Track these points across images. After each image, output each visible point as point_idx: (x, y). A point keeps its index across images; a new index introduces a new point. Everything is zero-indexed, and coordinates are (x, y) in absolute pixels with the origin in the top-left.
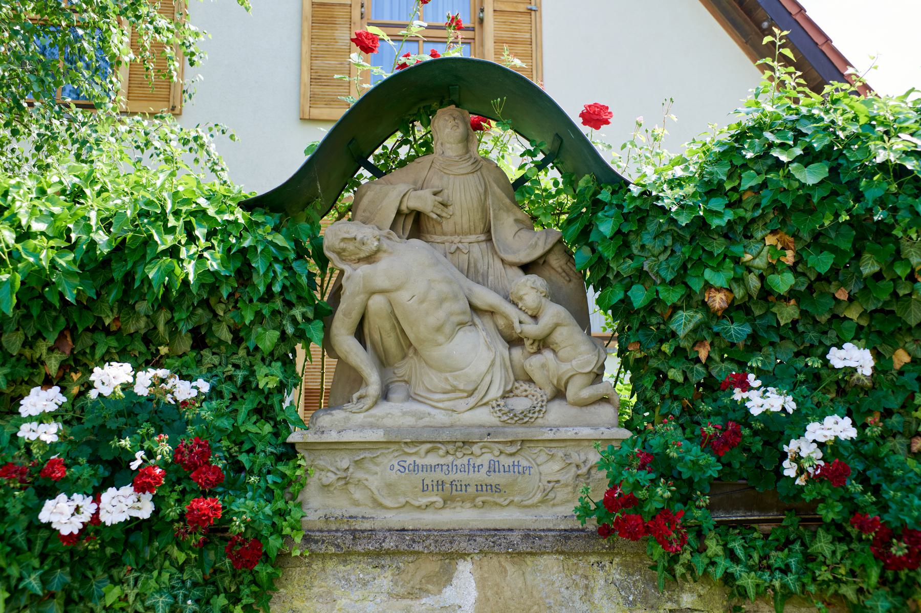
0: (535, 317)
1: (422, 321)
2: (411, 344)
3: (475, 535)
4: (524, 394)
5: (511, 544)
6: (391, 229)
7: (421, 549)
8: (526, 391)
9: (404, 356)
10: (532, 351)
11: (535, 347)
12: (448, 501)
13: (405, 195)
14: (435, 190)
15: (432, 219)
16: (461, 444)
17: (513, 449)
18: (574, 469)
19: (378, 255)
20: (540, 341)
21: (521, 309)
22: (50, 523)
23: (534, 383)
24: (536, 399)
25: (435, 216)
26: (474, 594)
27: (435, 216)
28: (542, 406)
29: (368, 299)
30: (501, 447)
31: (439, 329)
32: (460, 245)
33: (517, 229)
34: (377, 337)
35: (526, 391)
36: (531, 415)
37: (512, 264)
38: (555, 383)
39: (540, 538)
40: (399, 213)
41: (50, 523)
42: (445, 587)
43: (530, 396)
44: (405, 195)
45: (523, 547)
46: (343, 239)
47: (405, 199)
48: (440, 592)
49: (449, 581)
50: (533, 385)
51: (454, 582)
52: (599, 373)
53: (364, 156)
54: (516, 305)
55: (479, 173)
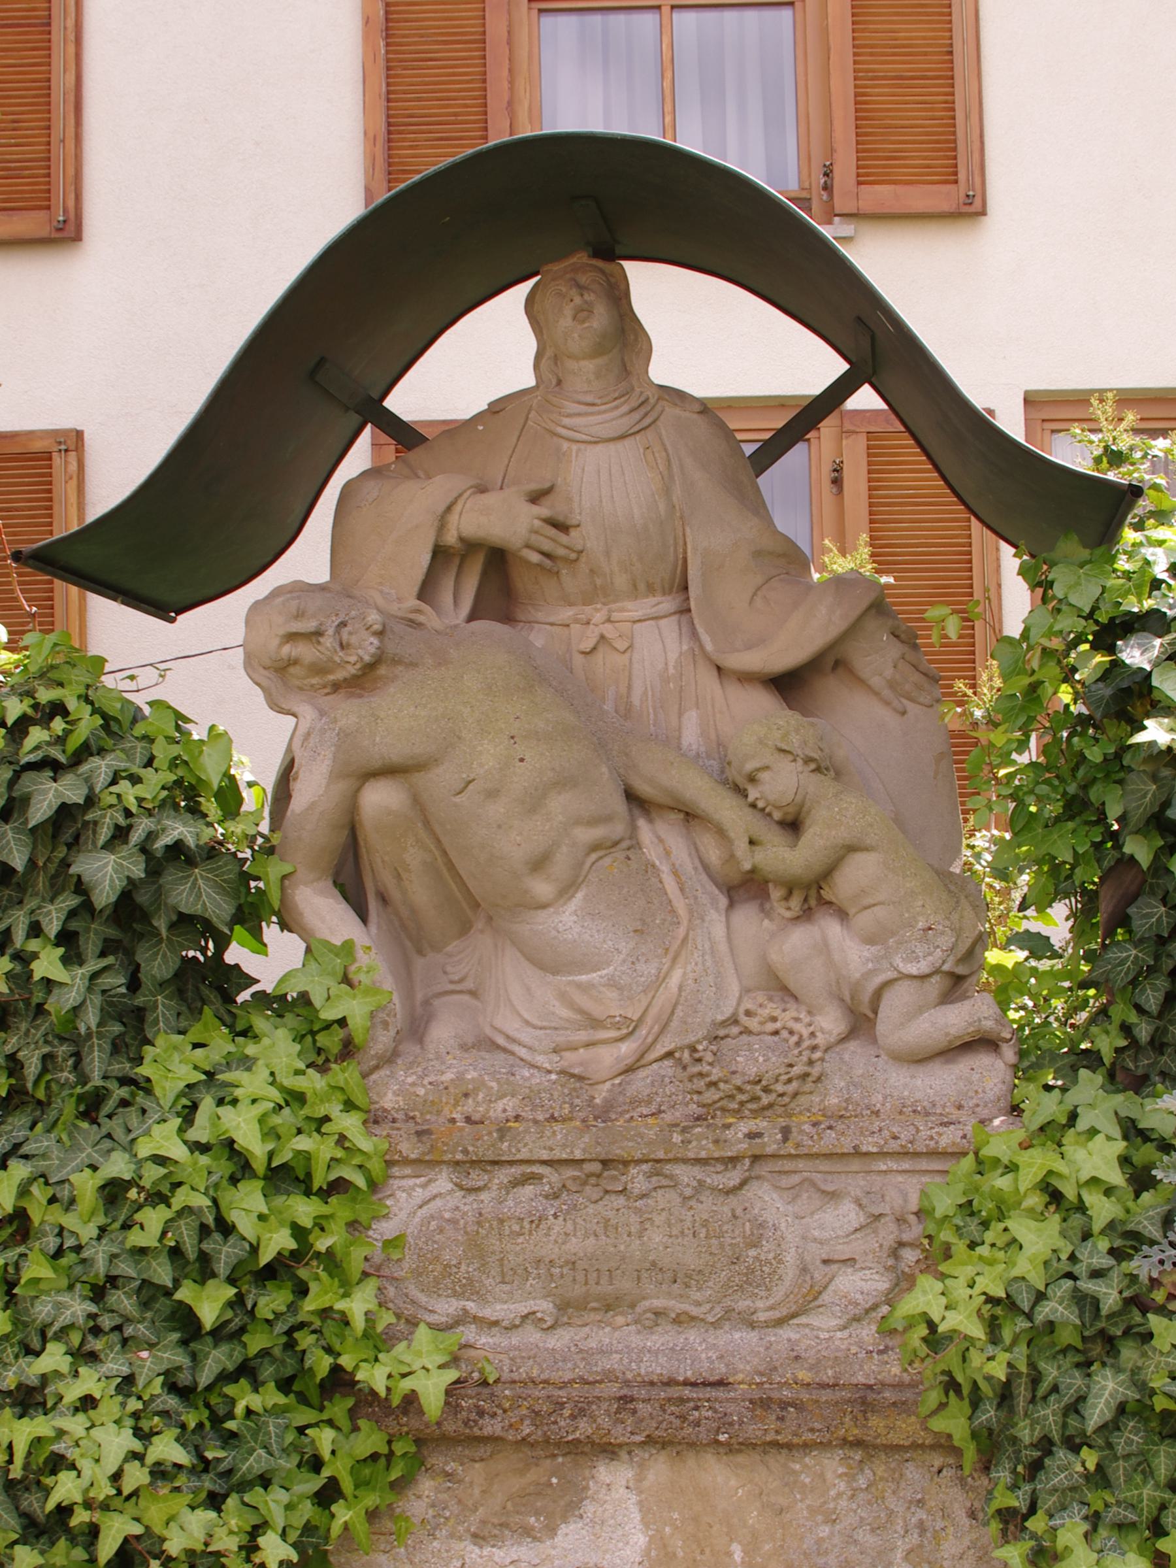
0: (793, 826)
1: (504, 836)
2: (477, 905)
3: (632, 1399)
4: (770, 1027)
5: (724, 1422)
6: (421, 596)
7: (498, 1431)
8: (774, 1019)
9: (465, 928)
10: (788, 914)
11: (796, 902)
12: (569, 1309)
13: (449, 509)
14: (534, 486)
15: (528, 563)
16: (596, 1167)
17: (733, 1177)
18: (893, 1227)
19: (382, 670)
20: (808, 887)
21: (753, 806)
22: (1048, 938)
23: (796, 998)
24: (798, 1044)
25: (535, 558)
26: (640, 1539)
27: (535, 558)
28: (811, 1063)
29: (358, 790)
30: (697, 1172)
31: (539, 864)
32: (609, 630)
33: (759, 580)
34: (387, 879)
35: (774, 1019)
36: (780, 1088)
37: (746, 678)
38: (847, 998)
39: (799, 1406)
40: (440, 553)
41: (1048, 938)
42: (565, 1520)
43: (785, 1034)
44: (449, 509)
45: (753, 1431)
46: (292, 637)
47: (453, 518)
48: (552, 1531)
49: (572, 1509)
50: (792, 1005)
51: (589, 1508)
52: (961, 970)
53: (375, 395)
54: (741, 792)
55: (650, 434)
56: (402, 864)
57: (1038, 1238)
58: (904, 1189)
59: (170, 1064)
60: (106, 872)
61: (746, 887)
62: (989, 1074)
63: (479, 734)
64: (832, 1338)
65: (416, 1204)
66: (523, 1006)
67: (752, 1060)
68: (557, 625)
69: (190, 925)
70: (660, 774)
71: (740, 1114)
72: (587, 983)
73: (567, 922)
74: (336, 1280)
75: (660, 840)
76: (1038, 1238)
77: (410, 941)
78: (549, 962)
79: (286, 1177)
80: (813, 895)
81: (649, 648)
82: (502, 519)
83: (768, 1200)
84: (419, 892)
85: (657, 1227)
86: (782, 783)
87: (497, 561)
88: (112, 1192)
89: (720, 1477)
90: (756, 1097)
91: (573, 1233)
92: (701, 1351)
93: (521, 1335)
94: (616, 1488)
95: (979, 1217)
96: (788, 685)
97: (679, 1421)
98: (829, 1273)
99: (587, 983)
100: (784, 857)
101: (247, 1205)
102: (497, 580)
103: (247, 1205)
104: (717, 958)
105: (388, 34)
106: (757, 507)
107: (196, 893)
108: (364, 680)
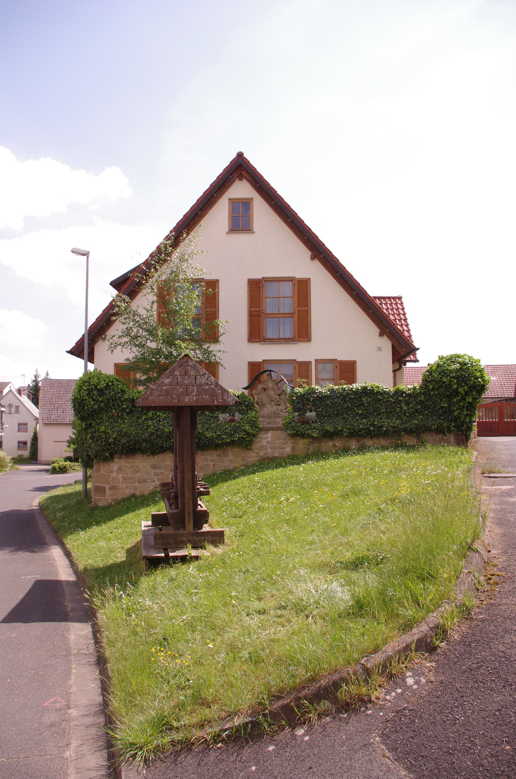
56: (260, 403)
57: (288, 420)
58: (283, 418)
59: (250, 412)
60: (246, 403)
61: (276, 405)
62: (287, 413)
63: (264, 397)
64: (280, 425)
65: (261, 419)
66: (266, 410)
67: (276, 413)
68: (268, 392)
69: (250, 406)
70: (272, 399)
71: (276, 415)
72: (269, 409)
73: (268, 406)
74: (206, 544)
75: (272, 402)
76: (288, 420)
77: (260, 407)
78: (267, 408)
79: (255, 417)
80: (279, 405)
81: (272, 393)
82: (265, 387)
83: (277, 419)
84: (261, 405)
85: (272, 420)
86: (278, 400)
87: (265, 389)
88: (248, 417)
89: (274, 432)
90: (276, 414)
91: (268, 420)
92: (274, 426)
93: (266, 425)
94: (270, 432)
95: (286, 419)
96: (279, 395)
97: (273, 429)
98: (280, 422)
99: (269, 409)
100: (278, 403)
101: (253, 418)
102: (265, 390)
103: (253, 418)
104: (275, 408)
105: (250, 322)
106: (278, 386)
107: (250, 404)
108: (258, 394)
